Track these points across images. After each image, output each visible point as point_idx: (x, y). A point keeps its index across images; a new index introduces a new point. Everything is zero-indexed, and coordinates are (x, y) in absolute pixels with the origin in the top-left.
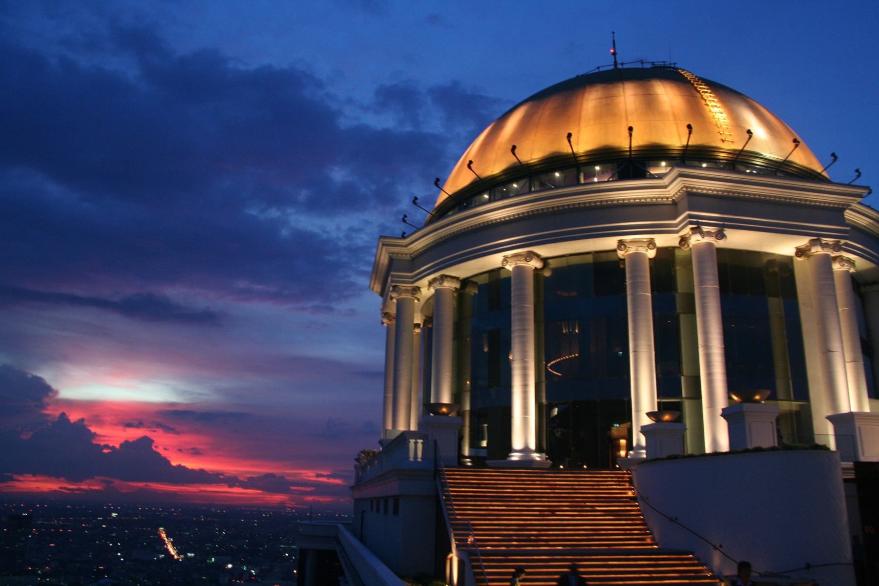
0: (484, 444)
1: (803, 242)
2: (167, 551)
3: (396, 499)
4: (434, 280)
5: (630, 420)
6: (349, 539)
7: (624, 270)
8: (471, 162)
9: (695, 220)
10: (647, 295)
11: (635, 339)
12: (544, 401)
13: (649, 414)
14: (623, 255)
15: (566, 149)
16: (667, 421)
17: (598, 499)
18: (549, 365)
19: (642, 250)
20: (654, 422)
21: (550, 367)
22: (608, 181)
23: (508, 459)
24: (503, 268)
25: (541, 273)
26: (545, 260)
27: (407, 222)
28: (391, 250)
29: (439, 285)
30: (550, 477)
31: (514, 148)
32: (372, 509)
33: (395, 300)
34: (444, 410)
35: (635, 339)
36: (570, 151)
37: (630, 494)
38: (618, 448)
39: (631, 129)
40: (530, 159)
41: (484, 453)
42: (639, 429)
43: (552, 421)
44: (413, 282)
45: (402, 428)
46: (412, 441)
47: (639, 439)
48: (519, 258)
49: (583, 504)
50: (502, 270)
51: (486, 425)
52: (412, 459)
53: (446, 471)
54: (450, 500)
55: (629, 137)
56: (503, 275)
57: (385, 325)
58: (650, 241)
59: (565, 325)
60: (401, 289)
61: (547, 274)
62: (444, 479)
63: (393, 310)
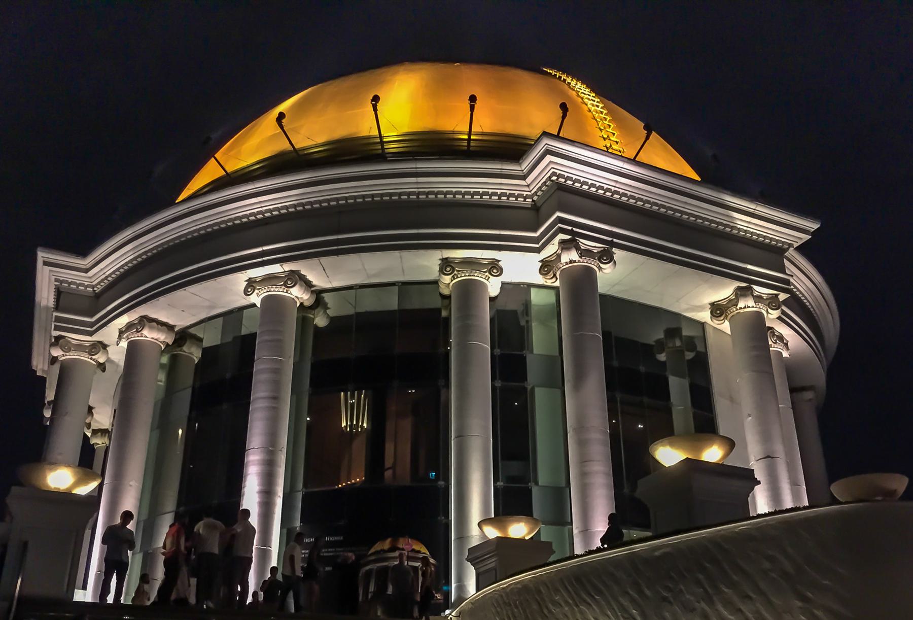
1: (725, 291)
4: (129, 326)
7: (447, 320)
9: (570, 228)
12: (297, 524)
26: (318, 294)
60: (70, 342)
61: (321, 321)
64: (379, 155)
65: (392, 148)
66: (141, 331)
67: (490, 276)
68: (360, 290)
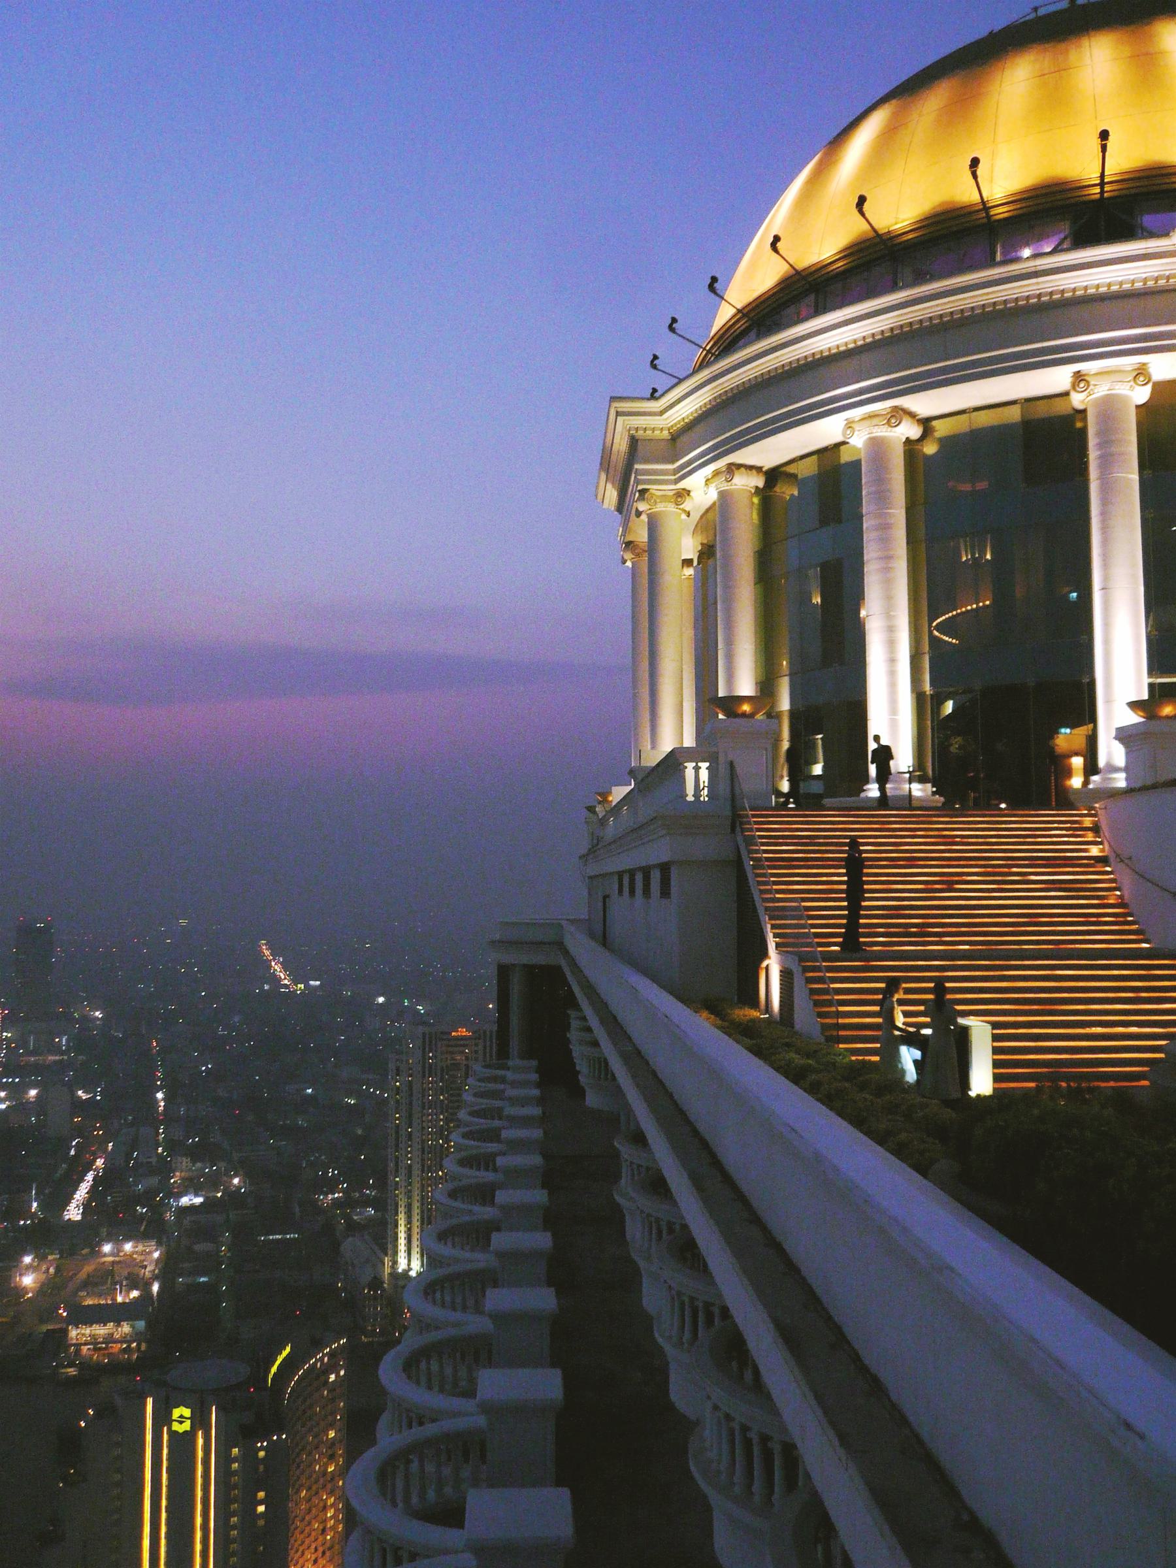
0: (818, 769)
2: (276, 980)
3: (665, 868)
5: (1093, 719)
6: (581, 947)
7: (1083, 432)
8: (777, 239)
10: (1130, 479)
11: (1106, 565)
12: (927, 688)
13: (1135, 705)
14: (1083, 401)
15: (966, 194)
16: (1167, 717)
17: (1033, 862)
18: (934, 624)
19: (1122, 389)
20: (1143, 720)
21: (937, 628)
22: (1055, 251)
23: (863, 795)
24: (844, 443)
25: (919, 447)
26: (926, 423)
27: (659, 367)
28: (634, 422)
29: (726, 484)
30: (942, 823)
31: (862, 200)
32: (621, 891)
33: (644, 517)
34: (746, 708)
35: (1106, 565)
36: (976, 198)
37: (1095, 851)
38: (1069, 773)
39: (1104, 135)
40: (894, 221)
41: (817, 788)
42: (1113, 734)
43: (944, 727)
44: (677, 481)
45: (667, 745)
46: (690, 766)
47: (1111, 752)
48: (875, 421)
49: (1006, 870)
50: (842, 448)
51: (820, 736)
52: (690, 798)
53: (754, 816)
54: (762, 867)
55: (1101, 154)
56: (845, 457)
57: (629, 564)
58: (1138, 369)
59: (966, 546)
61: (930, 449)
62: (751, 830)
63: (641, 535)
64: (984, 225)
65: (1001, 213)
66: (731, 480)
67: (1134, 385)
68: (975, 413)
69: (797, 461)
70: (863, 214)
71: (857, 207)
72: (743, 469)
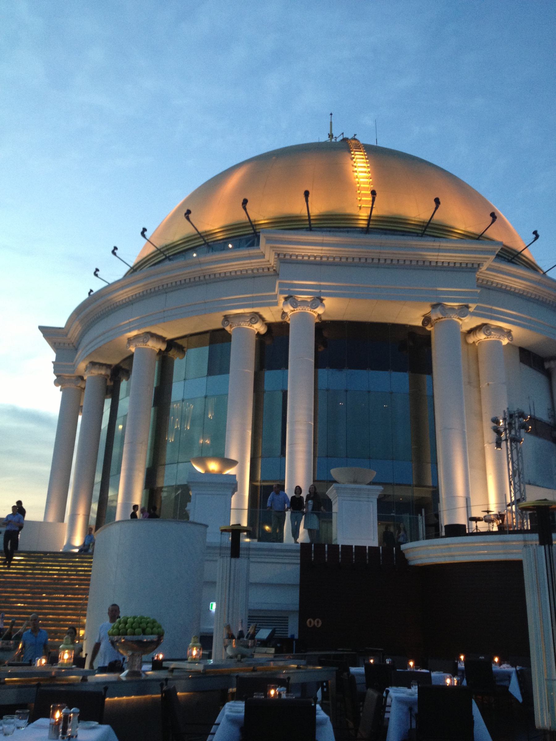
69: (188, 337)
70: (245, 209)
71: (242, 205)
72: (97, 366)
